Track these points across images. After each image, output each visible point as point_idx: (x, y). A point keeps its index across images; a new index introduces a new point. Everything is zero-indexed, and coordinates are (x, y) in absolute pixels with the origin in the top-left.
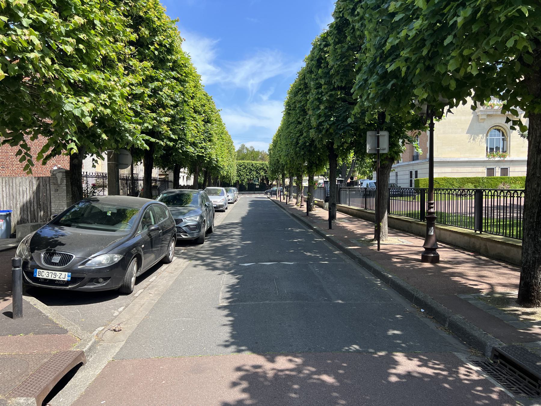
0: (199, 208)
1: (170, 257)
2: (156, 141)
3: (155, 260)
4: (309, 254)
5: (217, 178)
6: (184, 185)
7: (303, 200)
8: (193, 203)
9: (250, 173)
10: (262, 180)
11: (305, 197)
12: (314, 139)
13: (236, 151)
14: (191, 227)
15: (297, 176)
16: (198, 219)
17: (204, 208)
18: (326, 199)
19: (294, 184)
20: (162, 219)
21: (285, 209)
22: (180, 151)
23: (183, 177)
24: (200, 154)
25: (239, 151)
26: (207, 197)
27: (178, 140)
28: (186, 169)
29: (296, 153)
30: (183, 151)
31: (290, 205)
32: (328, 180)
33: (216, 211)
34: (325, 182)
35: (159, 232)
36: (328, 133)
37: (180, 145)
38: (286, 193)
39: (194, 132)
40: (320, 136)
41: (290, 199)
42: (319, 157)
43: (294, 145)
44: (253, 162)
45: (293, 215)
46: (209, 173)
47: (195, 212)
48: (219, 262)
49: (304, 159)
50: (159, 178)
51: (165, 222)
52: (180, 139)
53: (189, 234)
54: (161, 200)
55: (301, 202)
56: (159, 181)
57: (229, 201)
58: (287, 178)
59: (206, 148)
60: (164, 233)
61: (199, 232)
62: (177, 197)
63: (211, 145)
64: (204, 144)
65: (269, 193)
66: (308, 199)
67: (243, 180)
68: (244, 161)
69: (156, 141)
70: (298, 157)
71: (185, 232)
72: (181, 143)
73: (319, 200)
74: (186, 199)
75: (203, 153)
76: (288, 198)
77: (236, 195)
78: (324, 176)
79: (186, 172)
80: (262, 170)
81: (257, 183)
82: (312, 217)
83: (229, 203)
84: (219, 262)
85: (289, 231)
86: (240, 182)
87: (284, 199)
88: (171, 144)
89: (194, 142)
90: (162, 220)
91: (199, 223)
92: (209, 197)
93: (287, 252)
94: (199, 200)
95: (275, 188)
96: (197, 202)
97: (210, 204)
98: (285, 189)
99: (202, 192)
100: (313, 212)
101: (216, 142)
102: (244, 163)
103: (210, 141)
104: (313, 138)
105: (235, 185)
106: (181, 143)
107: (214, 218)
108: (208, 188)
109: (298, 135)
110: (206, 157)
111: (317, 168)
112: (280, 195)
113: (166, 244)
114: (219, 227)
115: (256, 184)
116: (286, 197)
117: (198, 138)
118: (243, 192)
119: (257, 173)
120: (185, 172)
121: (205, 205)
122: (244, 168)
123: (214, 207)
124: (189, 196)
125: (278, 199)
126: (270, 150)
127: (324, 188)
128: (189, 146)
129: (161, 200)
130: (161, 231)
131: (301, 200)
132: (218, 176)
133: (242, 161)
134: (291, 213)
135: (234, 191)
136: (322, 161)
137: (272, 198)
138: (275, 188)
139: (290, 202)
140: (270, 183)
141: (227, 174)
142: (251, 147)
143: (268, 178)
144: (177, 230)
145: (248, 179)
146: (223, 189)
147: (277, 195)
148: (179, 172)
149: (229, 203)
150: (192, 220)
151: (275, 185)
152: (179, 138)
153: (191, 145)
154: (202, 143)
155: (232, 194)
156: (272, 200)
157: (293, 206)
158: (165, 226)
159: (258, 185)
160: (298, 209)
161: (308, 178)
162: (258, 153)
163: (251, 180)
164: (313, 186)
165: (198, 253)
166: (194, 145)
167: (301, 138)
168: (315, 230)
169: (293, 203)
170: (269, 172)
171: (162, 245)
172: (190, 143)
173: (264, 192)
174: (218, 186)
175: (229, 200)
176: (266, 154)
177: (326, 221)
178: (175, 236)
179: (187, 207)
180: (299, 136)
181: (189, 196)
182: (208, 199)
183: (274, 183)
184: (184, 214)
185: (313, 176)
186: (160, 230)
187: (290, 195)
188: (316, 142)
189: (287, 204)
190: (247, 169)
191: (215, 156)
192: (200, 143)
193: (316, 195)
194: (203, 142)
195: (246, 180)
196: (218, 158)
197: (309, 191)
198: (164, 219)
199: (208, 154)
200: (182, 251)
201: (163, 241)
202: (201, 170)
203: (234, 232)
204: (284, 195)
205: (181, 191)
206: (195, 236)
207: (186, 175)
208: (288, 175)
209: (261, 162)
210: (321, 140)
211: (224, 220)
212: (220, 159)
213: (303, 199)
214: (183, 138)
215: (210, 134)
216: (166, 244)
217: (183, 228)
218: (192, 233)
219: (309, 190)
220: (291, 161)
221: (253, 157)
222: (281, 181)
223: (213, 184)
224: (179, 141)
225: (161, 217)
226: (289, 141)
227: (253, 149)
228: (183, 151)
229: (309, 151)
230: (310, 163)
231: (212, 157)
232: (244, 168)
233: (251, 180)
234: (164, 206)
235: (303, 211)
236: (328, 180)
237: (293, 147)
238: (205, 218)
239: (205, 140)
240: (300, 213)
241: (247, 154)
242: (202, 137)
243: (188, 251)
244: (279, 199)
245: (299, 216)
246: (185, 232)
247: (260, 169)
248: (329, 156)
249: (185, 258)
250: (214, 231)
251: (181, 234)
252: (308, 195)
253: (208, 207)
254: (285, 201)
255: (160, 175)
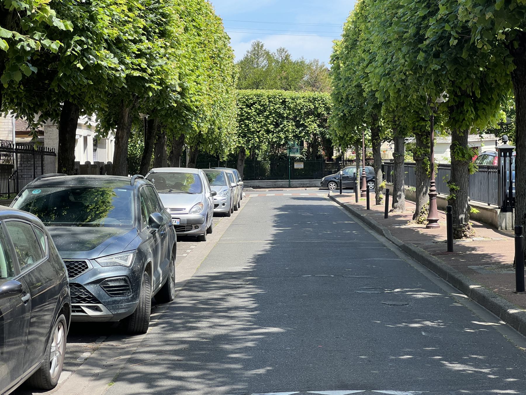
0: (133, 231)
1: (53, 371)
2: (14, 36)
3: (12, 379)
4: (458, 367)
5: (181, 141)
6: (88, 163)
7: (435, 206)
8: (116, 215)
9: (277, 125)
10: (313, 145)
11: (442, 195)
12: (470, 24)
13: (236, 61)
14: (111, 284)
15: (417, 134)
16: (129, 260)
17: (147, 231)
18: (505, 202)
19: (409, 159)
20: (30, 261)
21: (381, 233)
22: (79, 65)
23: (85, 139)
24: (136, 74)
25: (246, 63)
26: (156, 196)
27: (74, 33)
28: (94, 117)
29: (415, 68)
30: (87, 67)
31: (396, 221)
32: (510, 145)
33: (182, 238)
34: (500, 150)
35: (24, 299)
36: (511, 7)
37: (79, 48)
38: (383, 183)
39: (119, 10)
40: (489, 15)
41: (395, 201)
42: (483, 78)
43: (409, 44)
44: (287, 94)
45: (406, 250)
46: (159, 127)
47: (120, 239)
48: (197, 386)
49: (437, 84)
50: (17, 144)
51: (39, 269)
52: (79, 30)
53: (106, 304)
54: (26, 207)
55: (430, 210)
56: (17, 151)
57: (218, 210)
58: (386, 139)
59: (151, 55)
60: (36, 302)
61: (134, 299)
62: (72, 198)
63: (166, 48)
64: (146, 44)
65: (332, 186)
66: (451, 201)
67: (258, 148)
68: (259, 92)
69: (14, 36)
70: (419, 80)
71: (95, 300)
72: (80, 43)
73: (484, 205)
74: (97, 203)
75: (144, 70)
76: (391, 198)
77: (235, 190)
78: (497, 133)
79: (94, 124)
80: (312, 118)
81: (298, 156)
82: (463, 257)
83: (216, 215)
84: (197, 386)
85: (395, 297)
86: (247, 152)
87: (378, 202)
88: (55, 46)
89: (118, 40)
90: (32, 265)
91: (133, 271)
92: (161, 196)
93: (392, 360)
94: (134, 208)
95: (351, 170)
96: (127, 212)
97: (165, 217)
98: (380, 172)
99: (140, 183)
100: (465, 242)
101: (180, 38)
102: (258, 96)
103: (163, 34)
104: (467, 21)
105: (232, 163)
106: (80, 43)
107: (174, 258)
108: (156, 170)
109: (421, 13)
110: (152, 81)
111: (476, 109)
112: (368, 191)
113: (41, 334)
114: (189, 285)
115: (293, 158)
116: (384, 197)
117: (130, 26)
118: (256, 183)
119: (298, 125)
120: (89, 127)
121: (151, 221)
122: (260, 112)
123: (176, 227)
124: (103, 193)
125: (359, 203)
126: (335, 58)
127: (499, 170)
128: (104, 52)
129: (26, 207)
130: (28, 296)
131: (431, 204)
132: (183, 137)
133: (255, 91)
134: (401, 242)
135: (230, 180)
136: (491, 90)
137: (341, 200)
138: (351, 170)
139: (397, 212)
140: (335, 154)
141: (211, 131)
142: (281, 51)
143: (329, 141)
144: (72, 293)
145: (271, 144)
146: (200, 172)
147: (356, 192)
148: (75, 125)
149: (216, 215)
150: (114, 264)
151: (351, 161)
152: (76, 27)
153: (109, 48)
154: (141, 41)
155: (224, 188)
156: (342, 205)
157: (405, 222)
158: (38, 281)
159: (300, 160)
160: (422, 231)
161: (449, 139)
162: (300, 67)
163: (279, 145)
164: (467, 163)
165: (131, 361)
166: (120, 48)
167: (432, 21)
168: (473, 294)
169: (405, 213)
170: (333, 123)
171: (30, 337)
172: (106, 40)
173: (318, 182)
174: (184, 166)
175: (216, 206)
176: (322, 70)
177: (506, 267)
178: (65, 310)
179: (98, 225)
180: (424, 18)
181: (103, 193)
182: (157, 204)
183: (349, 154)
184: (90, 247)
185: (466, 133)
186: (24, 294)
187: (396, 190)
188: (476, 37)
189: (386, 216)
190: (267, 113)
191: (177, 77)
192: (135, 42)
193: (475, 189)
194: (144, 38)
195: (264, 147)
196: (185, 85)
197: (454, 179)
198: (35, 260)
199: (158, 73)
200: (86, 355)
201: (32, 324)
202: (135, 119)
203: (231, 299)
204: (377, 190)
205: (81, 181)
206: (123, 311)
207: (93, 134)
208: (389, 132)
209: (308, 93)
210: (492, 26)
211: (202, 266)
212: (190, 84)
213: (435, 201)
214: (88, 29)
215: (163, 15)
216: (41, 334)
217: (90, 288)
218: (115, 302)
219: (453, 175)
220: (399, 90)
221: (287, 78)
222: (370, 150)
223: (170, 159)
224: (76, 38)
225: (27, 255)
226: (392, 33)
227: (287, 58)
228: (87, 67)
229: (456, 61)
230: (456, 95)
231: (169, 82)
232: (260, 112)
233: (279, 145)
234: (36, 223)
235: (434, 236)
236: (510, 145)
237: (405, 49)
238: (150, 259)
239: (148, 32)
240: (427, 244)
241: (268, 72)
242: (142, 23)
243: (102, 354)
244: (362, 202)
245: (426, 254)
246: (95, 300)
247: (309, 113)
248: (514, 75)
249: (98, 377)
250: (177, 296)
251: (83, 305)
252: (452, 190)
253: (158, 226)
254: (383, 210)
255: (19, 134)
